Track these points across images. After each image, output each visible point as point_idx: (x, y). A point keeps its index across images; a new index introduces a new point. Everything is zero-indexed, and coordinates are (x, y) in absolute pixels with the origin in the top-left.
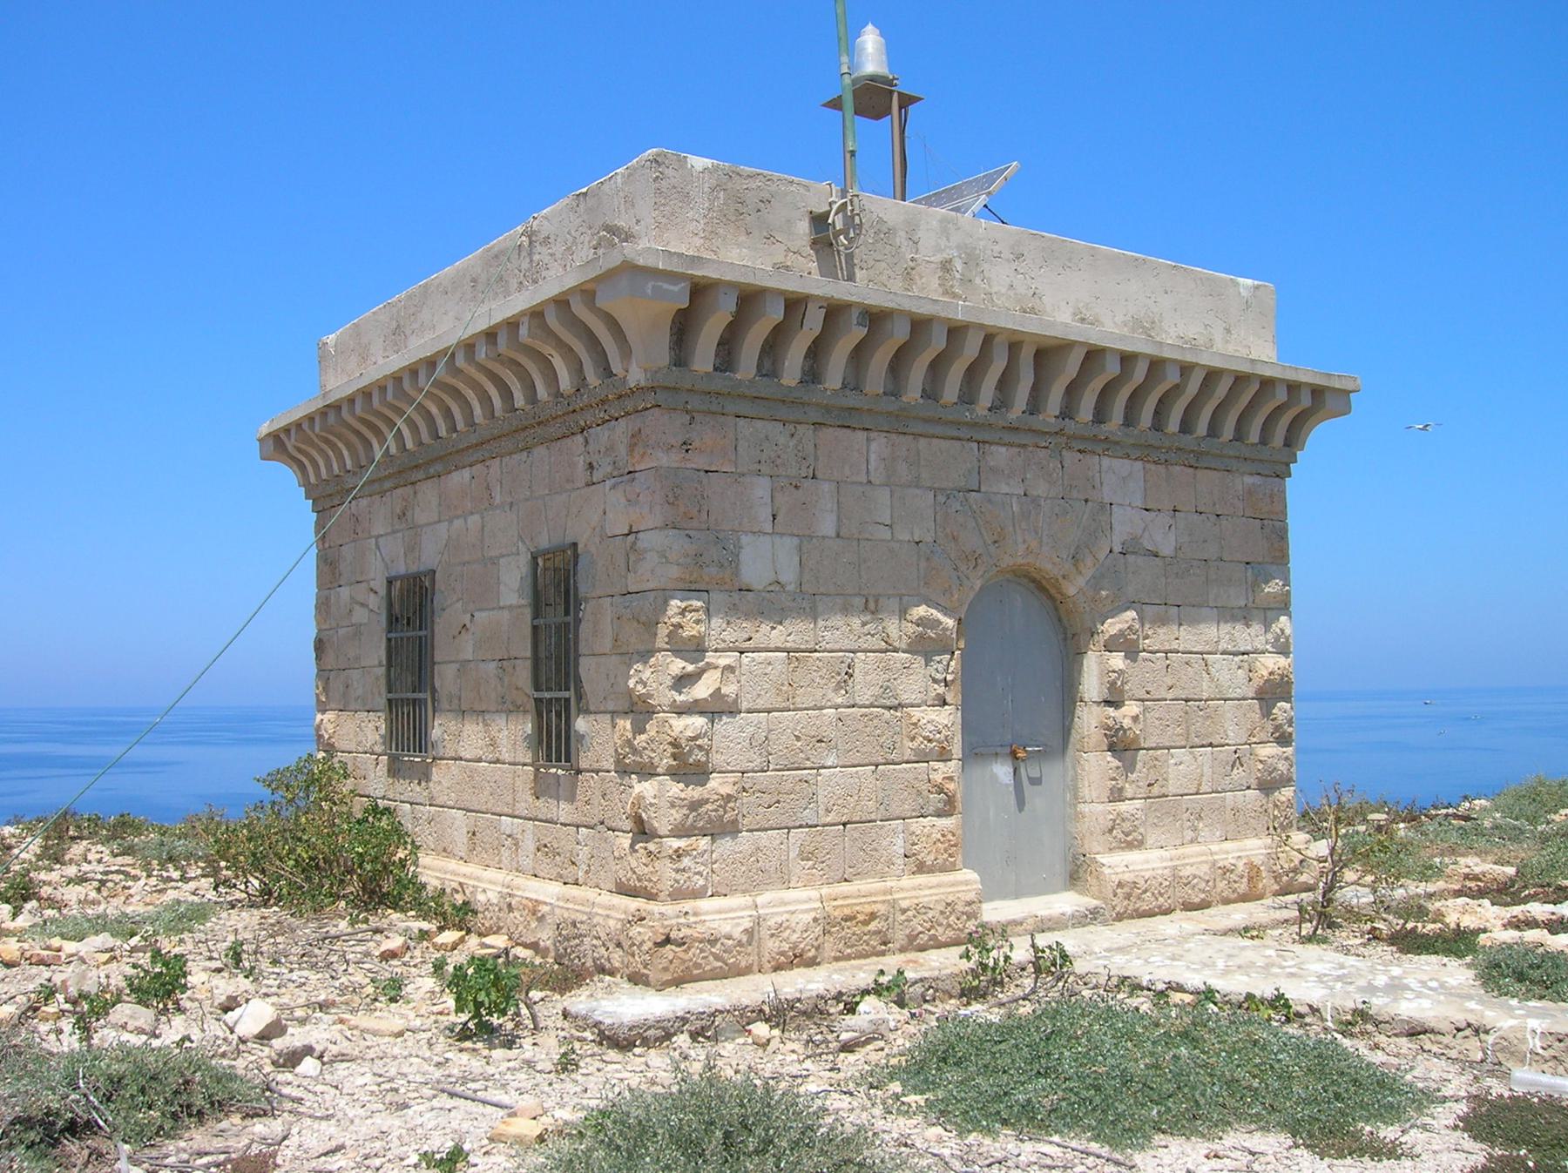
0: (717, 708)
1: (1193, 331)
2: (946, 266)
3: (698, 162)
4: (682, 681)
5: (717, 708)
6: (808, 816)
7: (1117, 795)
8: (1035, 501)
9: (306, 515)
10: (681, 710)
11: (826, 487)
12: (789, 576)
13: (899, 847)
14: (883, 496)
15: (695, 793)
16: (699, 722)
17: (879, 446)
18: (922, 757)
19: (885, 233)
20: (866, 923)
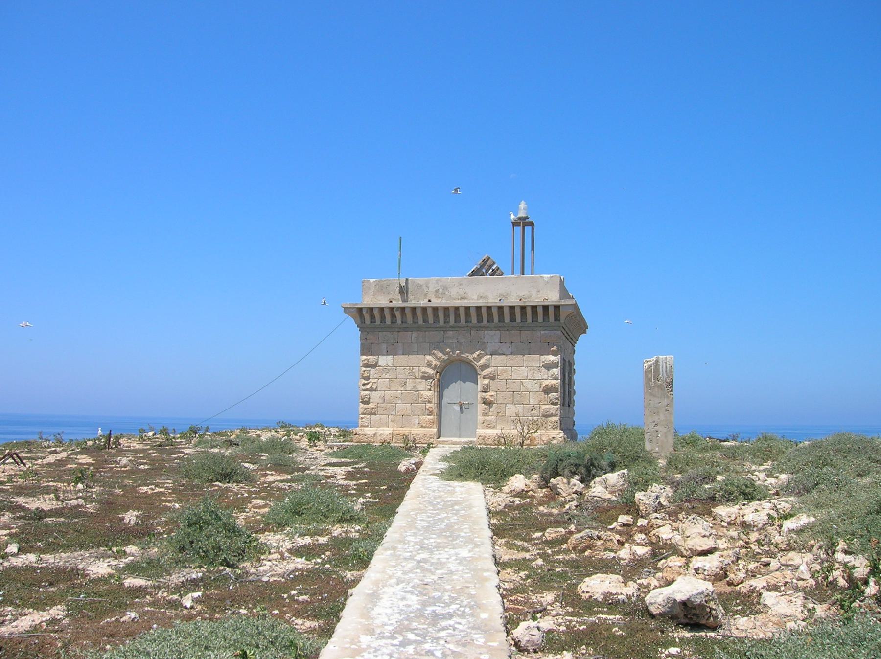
0: (371, 390)
1: (523, 293)
2: (437, 291)
3: (372, 280)
4: (364, 385)
5: (371, 390)
6: (393, 413)
7: (485, 414)
8: (461, 344)
9: (357, 333)
10: (364, 390)
11: (400, 344)
12: (390, 364)
13: (417, 421)
14: (416, 345)
15: (366, 406)
16: (367, 392)
17: (415, 334)
18: (424, 402)
19: (419, 286)
20: (704, 450)
